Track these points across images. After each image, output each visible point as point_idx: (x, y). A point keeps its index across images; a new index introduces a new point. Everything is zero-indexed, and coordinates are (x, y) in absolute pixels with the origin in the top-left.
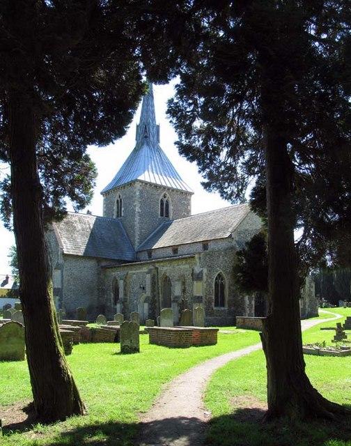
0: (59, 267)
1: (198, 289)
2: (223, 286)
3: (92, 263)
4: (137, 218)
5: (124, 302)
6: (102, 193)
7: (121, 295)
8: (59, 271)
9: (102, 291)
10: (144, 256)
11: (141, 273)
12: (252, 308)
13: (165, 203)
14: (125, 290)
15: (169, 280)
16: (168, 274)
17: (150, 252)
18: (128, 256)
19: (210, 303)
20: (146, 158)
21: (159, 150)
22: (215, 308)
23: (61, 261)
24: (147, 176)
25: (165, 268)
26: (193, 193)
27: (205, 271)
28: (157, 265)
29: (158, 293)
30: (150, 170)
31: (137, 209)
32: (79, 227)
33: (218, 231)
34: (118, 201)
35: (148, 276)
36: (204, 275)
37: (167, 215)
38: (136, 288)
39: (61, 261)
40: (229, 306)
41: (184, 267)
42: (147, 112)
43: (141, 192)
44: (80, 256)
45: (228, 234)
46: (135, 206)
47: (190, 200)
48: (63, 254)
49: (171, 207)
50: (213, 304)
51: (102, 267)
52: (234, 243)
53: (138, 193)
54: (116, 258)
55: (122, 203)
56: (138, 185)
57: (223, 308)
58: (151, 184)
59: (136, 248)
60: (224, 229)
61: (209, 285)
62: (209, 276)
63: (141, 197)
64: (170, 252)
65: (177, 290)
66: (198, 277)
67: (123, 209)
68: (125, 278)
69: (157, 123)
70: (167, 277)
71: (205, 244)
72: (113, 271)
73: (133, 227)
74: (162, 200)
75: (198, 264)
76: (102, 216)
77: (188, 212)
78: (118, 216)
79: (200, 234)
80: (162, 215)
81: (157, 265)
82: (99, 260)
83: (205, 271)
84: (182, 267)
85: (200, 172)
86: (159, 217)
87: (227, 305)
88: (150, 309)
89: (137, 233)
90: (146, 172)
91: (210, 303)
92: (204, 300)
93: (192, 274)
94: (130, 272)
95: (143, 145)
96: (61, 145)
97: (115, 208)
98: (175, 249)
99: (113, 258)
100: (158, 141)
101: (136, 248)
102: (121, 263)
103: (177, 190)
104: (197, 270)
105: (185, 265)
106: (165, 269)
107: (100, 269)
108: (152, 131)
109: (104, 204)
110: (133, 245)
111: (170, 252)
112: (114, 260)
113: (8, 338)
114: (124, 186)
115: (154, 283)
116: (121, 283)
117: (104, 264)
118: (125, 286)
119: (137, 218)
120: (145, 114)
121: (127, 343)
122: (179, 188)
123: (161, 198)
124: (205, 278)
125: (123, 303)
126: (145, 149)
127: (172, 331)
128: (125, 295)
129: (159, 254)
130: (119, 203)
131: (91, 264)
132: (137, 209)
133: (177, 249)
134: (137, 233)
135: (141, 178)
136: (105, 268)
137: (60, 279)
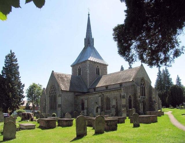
0: (60, 96)
1: (124, 102)
2: (131, 100)
3: (72, 94)
4: (88, 75)
5: (87, 109)
6: (71, 66)
8: (61, 97)
9: (76, 105)
10: (92, 90)
15: (109, 99)
16: (108, 97)
17: (95, 89)
18: (85, 90)
19: (127, 107)
21: (94, 48)
23: (61, 93)
24: (91, 59)
25: (107, 94)
26: (108, 65)
27: (125, 95)
28: (103, 93)
29: (104, 105)
30: (93, 57)
31: (88, 72)
32: (66, 79)
33: (126, 79)
34: (79, 69)
35: (100, 98)
37: (99, 74)
38: (93, 103)
39: (61, 93)
41: (116, 93)
43: (89, 65)
44: (67, 91)
45: (131, 80)
46: (87, 71)
47: (107, 68)
48: (62, 90)
49: (100, 71)
50: (128, 108)
51: (76, 95)
52: (134, 83)
53: (88, 65)
54: (81, 91)
56: (88, 62)
58: (93, 62)
59: (88, 87)
60: (129, 78)
61: (127, 100)
63: (89, 67)
64: (105, 88)
65: (114, 103)
66: (124, 97)
67: (81, 72)
68: (87, 99)
69: (93, 38)
70: (108, 98)
71: (121, 84)
72: (81, 97)
73: (86, 79)
75: (123, 92)
77: (106, 72)
78: (79, 75)
79: (118, 80)
80: (97, 74)
81: (103, 93)
82: (75, 92)
83: (125, 95)
84: (115, 93)
85: (17, 59)
89: (88, 81)
90: (91, 57)
93: (120, 96)
95: (88, 46)
97: (78, 72)
98: (107, 87)
99: (80, 91)
101: (88, 87)
102: (84, 93)
103: (102, 64)
104: (122, 94)
105: (117, 92)
106: (107, 95)
107: (75, 96)
108: (91, 41)
109: (72, 70)
110: (86, 86)
111: (105, 88)
112: (80, 92)
113: (98, 123)
114: (82, 63)
115: (102, 101)
117: (76, 94)
118: (88, 102)
119: (88, 75)
121: (136, 122)
122: (99, 62)
123: (96, 67)
126: (89, 49)
127: (144, 117)
128: (88, 106)
129: (98, 89)
131: (72, 94)
132: (88, 72)
133: (108, 87)
134: (88, 81)
135: (89, 59)
137: (61, 101)
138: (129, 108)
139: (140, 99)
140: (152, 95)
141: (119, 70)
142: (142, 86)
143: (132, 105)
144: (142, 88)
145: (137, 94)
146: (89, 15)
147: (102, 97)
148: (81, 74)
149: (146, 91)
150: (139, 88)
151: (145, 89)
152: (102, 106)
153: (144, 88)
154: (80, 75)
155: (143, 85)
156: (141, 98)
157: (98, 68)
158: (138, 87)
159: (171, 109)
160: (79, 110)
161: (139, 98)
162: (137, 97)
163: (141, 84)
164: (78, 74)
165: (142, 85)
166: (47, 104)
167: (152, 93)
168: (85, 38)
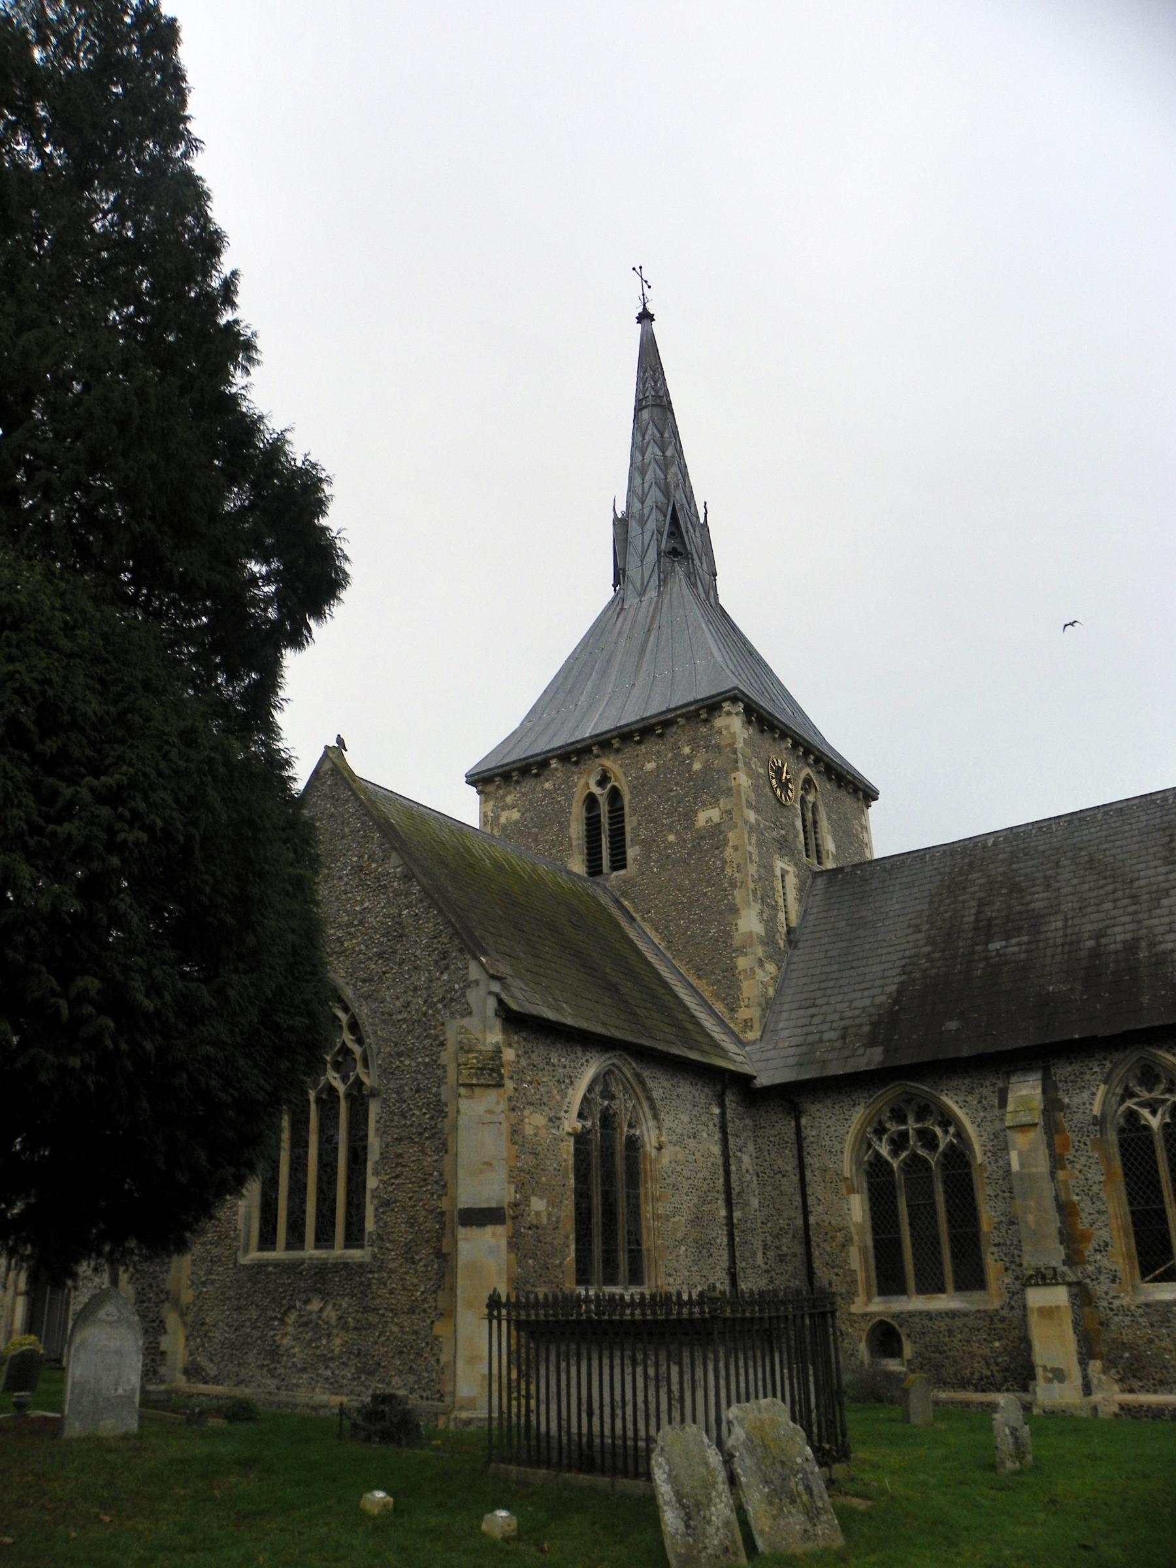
74: (591, 801)
146: (645, 317)
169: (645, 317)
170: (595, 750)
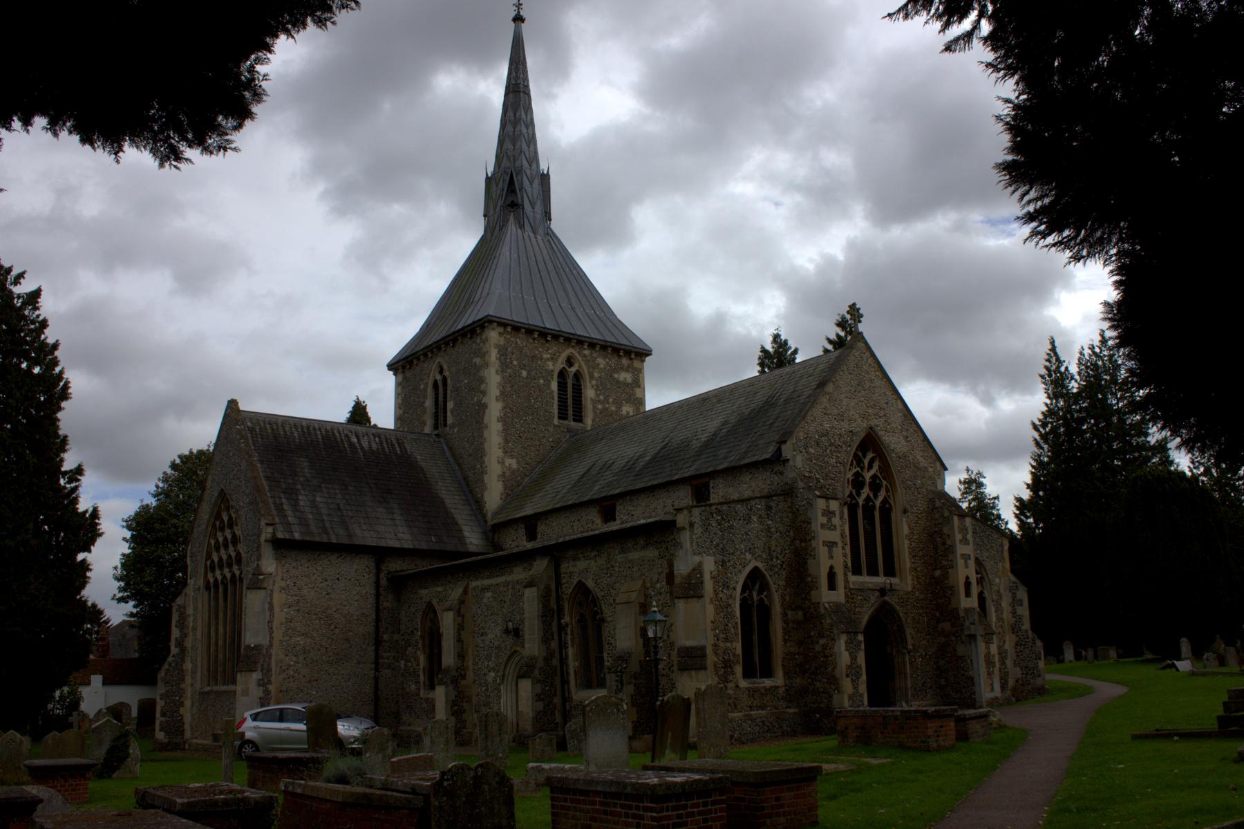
5: (457, 678)
7: (448, 659)
11: (507, 584)
12: (858, 676)
13: (394, 442)
14: (459, 640)
20: (624, 455)
22: (744, 684)
34: (435, 384)
35: (531, 594)
36: (707, 577)
37: (579, 418)
40: (787, 674)
42: (514, 141)
49: (589, 393)
50: (739, 670)
55: (449, 388)
57: (768, 683)
61: (723, 607)
62: (722, 582)
67: (450, 405)
69: (543, 167)
74: (562, 374)
76: (392, 427)
78: (436, 427)
80: (563, 416)
83: (709, 564)
86: (556, 421)
87: (780, 673)
88: (538, 697)
91: (727, 665)
92: (711, 658)
94: (474, 584)
96: (534, 357)
97: (429, 403)
100: (547, 215)
108: (531, 189)
110: (476, 504)
116: (447, 621)
118: (460, 627)
120: (509, 128)
124: (708, 585)
125: (455, 681)
128: (461, 656)
130: (440, 388)
136: (399, 584)
138: (748, 674)
139: (839, 596)
140: (952, 566)
141: (340, 414)
142: (861, 501)
143: (779, 647)
144: (869, 509)
145: (810, 562)
146: (518, 19)
147: (548, 588)
148: (450, 420)
149: (904, 530)
150: (828, 513)
151: (896, 515)
152: (547, 659)
153: (886, 511)
154: (445, 425)
155: (875, 487)
156: (851, 593)
157: (573, 369)
158: (821, 503)
159: (974, 662)
160: (413, 687)
161: (832, 586)
162: (814, 585)
163: (858, 483)
164: (430, 422)
165: (866, 491)
166: (188, 643)
167: (951, 549)
168: (491, 170)
169: (518, 19)
170: (561, 340)
